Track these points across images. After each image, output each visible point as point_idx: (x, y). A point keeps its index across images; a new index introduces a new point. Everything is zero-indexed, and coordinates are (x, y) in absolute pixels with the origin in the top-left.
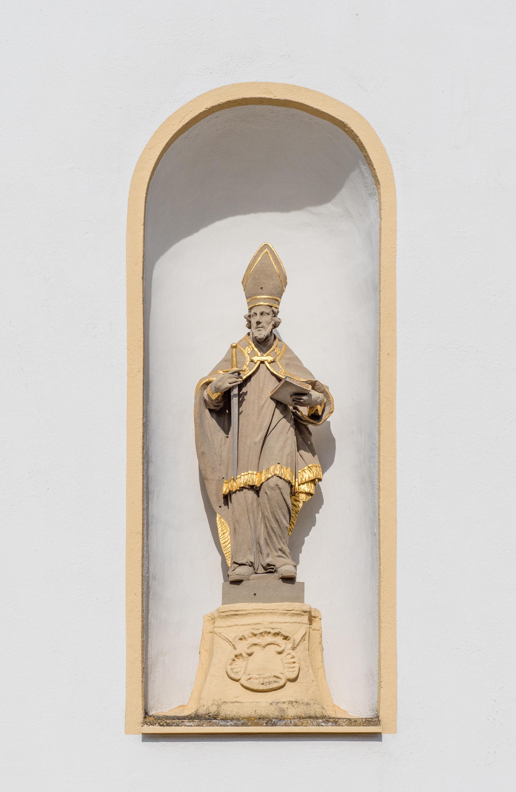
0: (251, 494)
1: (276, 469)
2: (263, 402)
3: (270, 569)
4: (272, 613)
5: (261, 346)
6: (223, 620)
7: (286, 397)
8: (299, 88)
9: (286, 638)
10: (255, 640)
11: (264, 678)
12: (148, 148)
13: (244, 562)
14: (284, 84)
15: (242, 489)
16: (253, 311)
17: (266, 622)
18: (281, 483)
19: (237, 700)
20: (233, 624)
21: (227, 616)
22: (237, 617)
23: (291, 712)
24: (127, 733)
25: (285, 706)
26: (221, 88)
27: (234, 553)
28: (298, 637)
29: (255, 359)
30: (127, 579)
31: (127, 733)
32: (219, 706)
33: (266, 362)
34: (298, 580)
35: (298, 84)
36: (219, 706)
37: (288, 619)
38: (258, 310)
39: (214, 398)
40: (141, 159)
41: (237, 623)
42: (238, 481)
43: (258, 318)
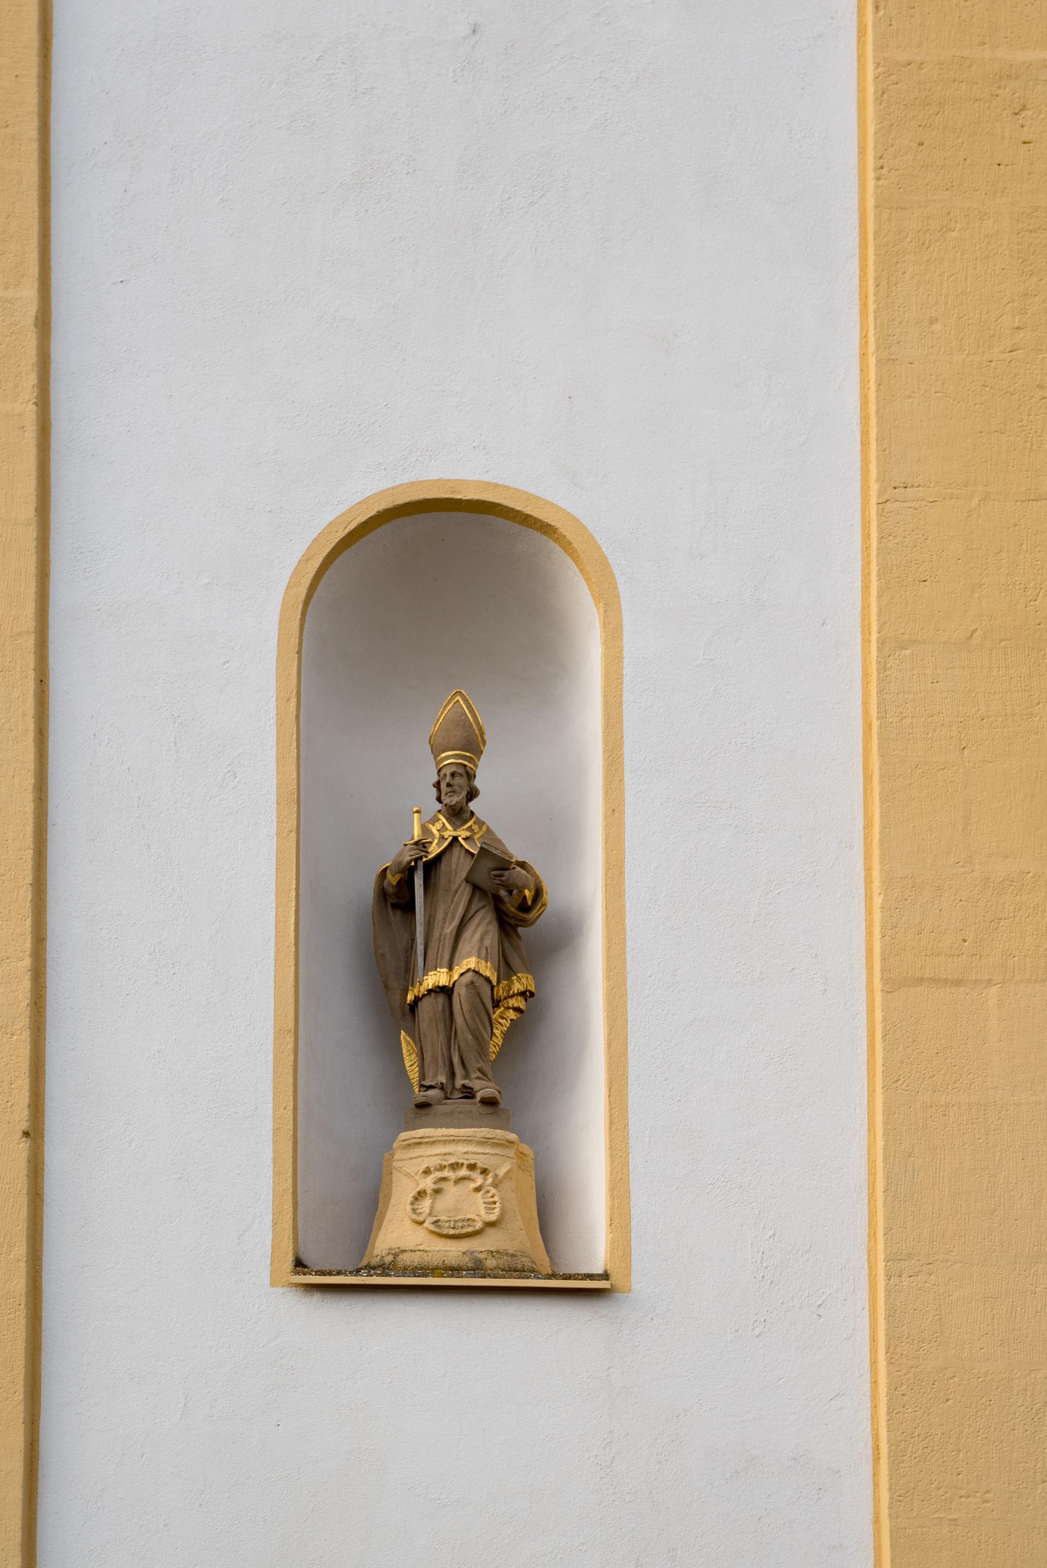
0: (441, 999)
1: (471, 962)
2: (456, 886)
3: (468, 1093)
4: (468, 1141)
5: (454, 820)
6: (405, 1151)
7: (483, 878)
8: (496, 485)
9: (484, 1172)
10: (446, 1173)
11: (455, 1221)
12: (305, 559)
13: (433, 1084)
14: (478, 481)
15: (430, 991)
16: (442, 774)
17: (460, 1152)
18: (480, 982)
19: (421, 1248)
20: (417, 1154)
21: (409, 1145)
22: (423, 1146)
23: (491, 1263)
24: (273, 1284)
25: (482, 1256)
26: (398, 486)
27: (423, 1076)
28: (502, 1172)
29: (446, 834)
30: (274, 1088)
31: (273, 1284)
32: (396, 1255)
33: (460, 839)
34: (502, 1106)
35: (494, 481)
36: (396, 1255)
37: (487, 1150)
38: (448, 771)
39: (394, 883)
40: (296, 573)
41: (421, 1154)
42: (425, 984)
43: (448, 779)
